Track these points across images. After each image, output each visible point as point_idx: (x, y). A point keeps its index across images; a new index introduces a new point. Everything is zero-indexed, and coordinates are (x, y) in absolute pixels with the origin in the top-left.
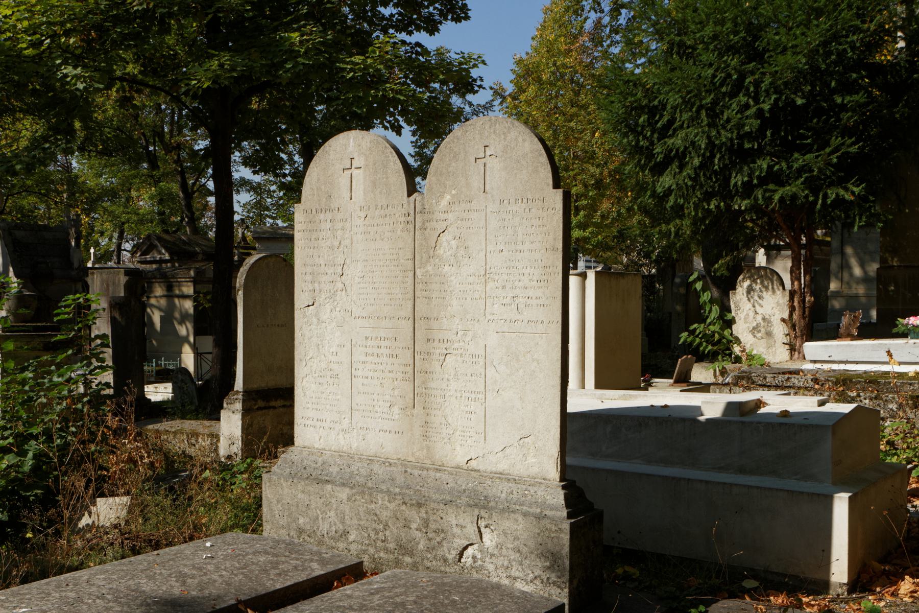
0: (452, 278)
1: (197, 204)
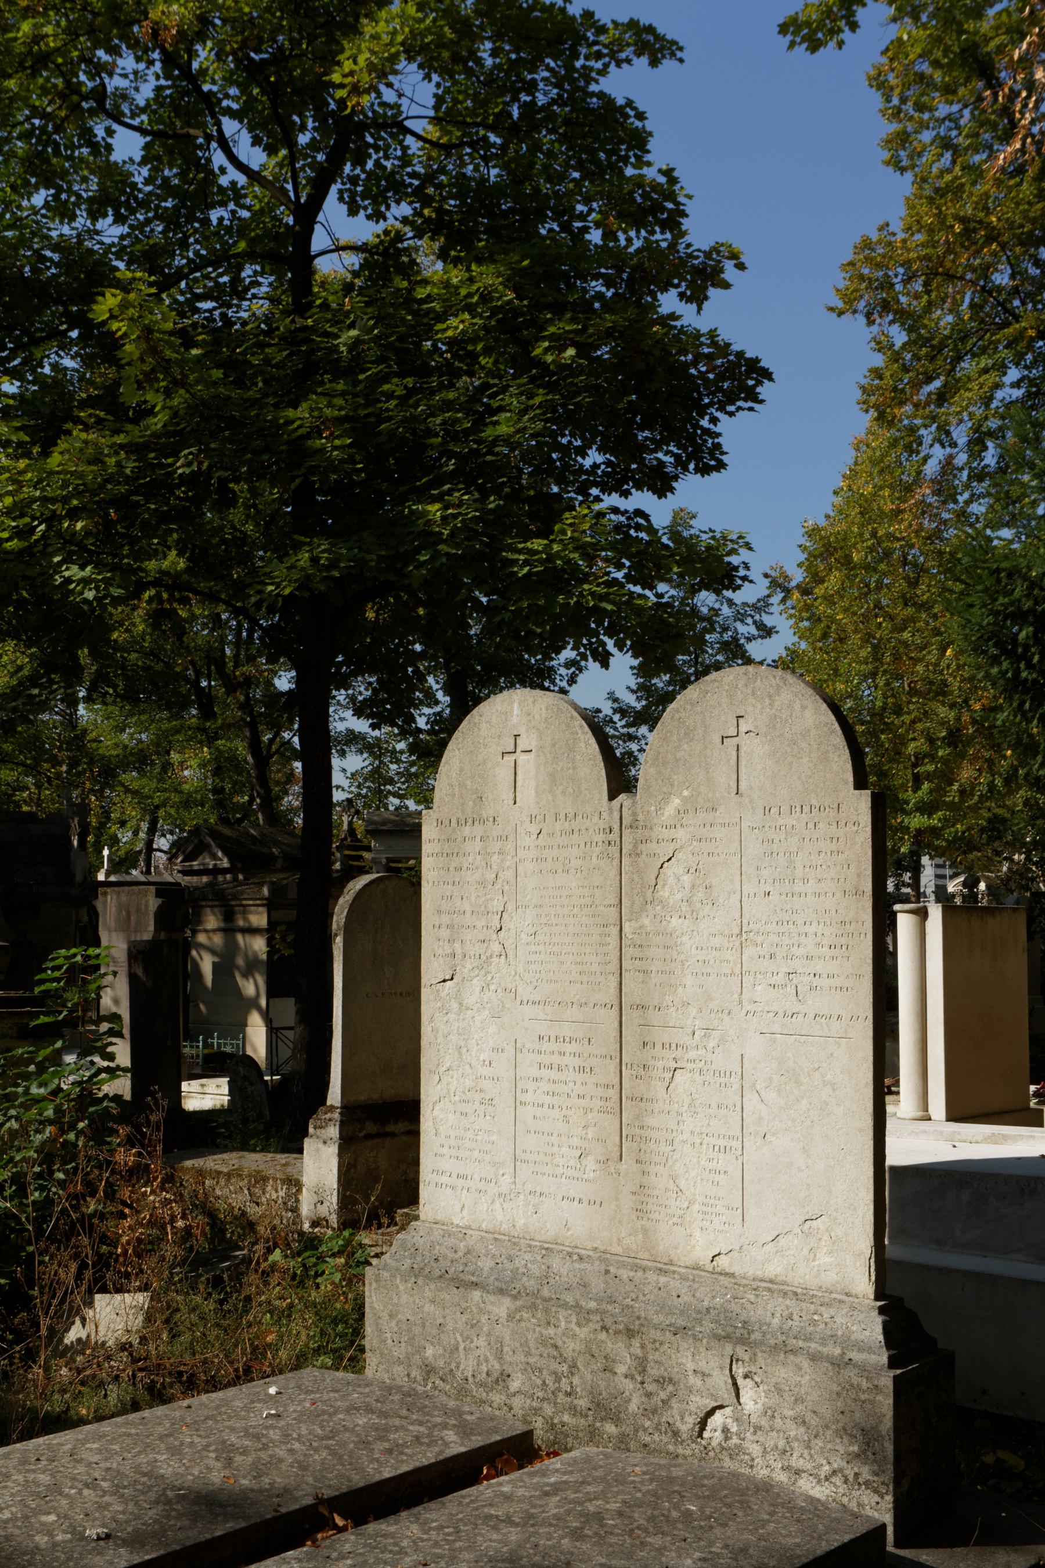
0: (684, 939)
1: (275, 773)
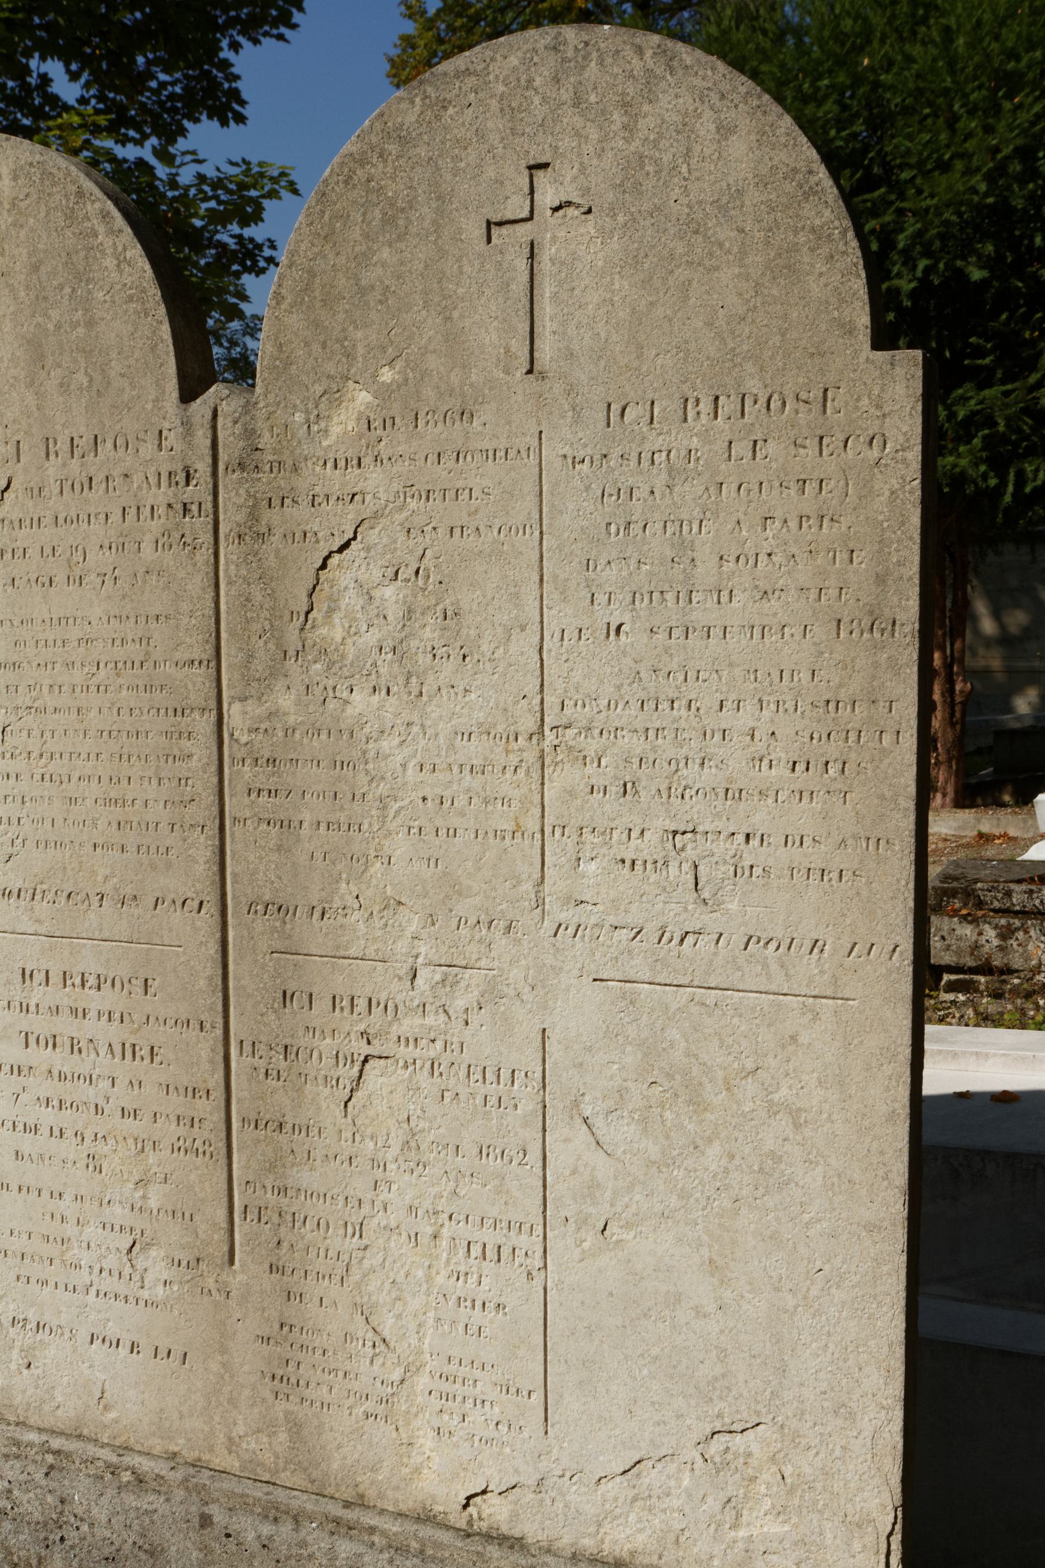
0: (385, 745)
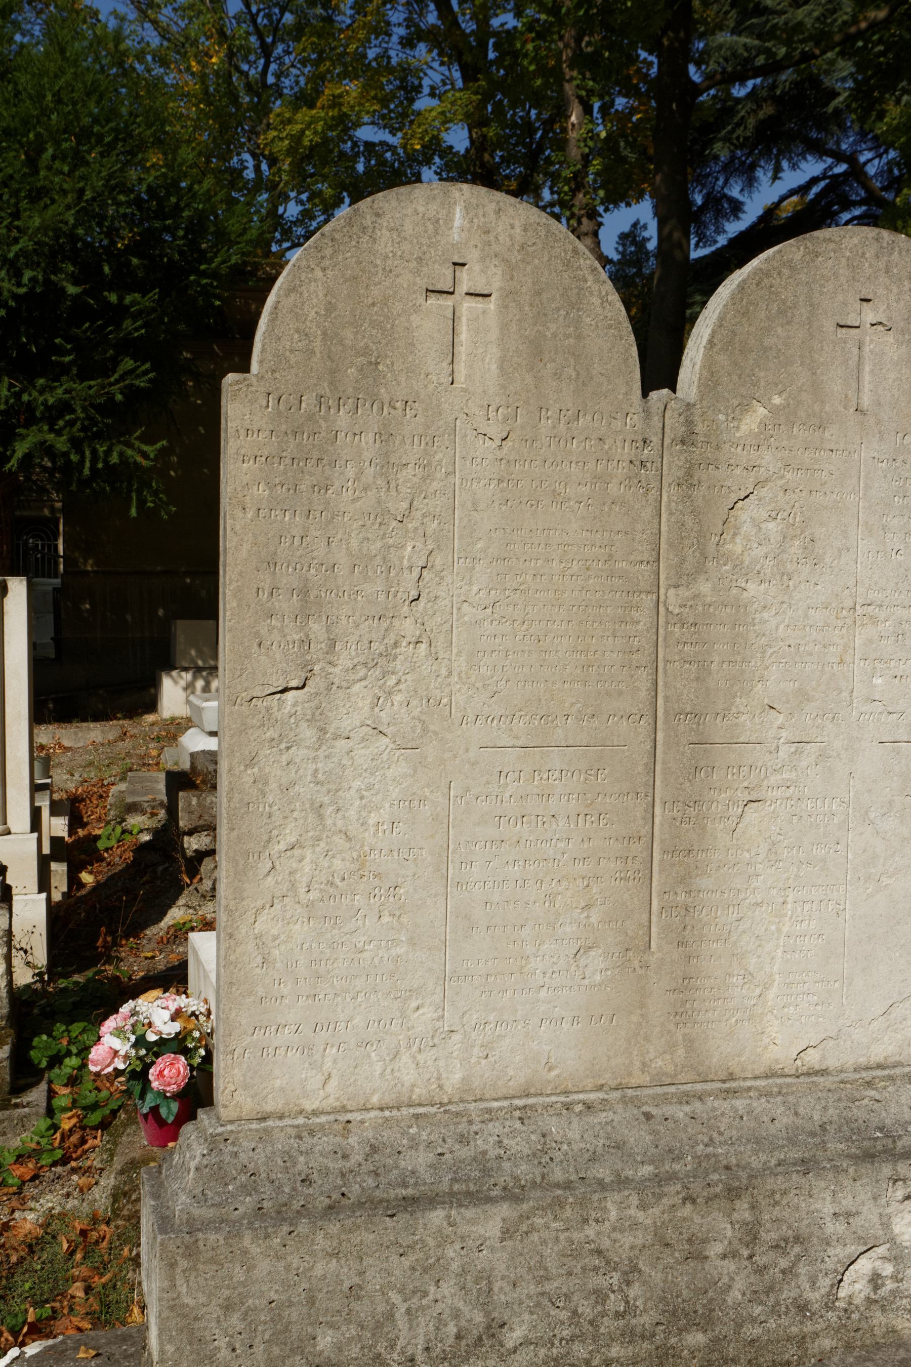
0: (765, 615)
